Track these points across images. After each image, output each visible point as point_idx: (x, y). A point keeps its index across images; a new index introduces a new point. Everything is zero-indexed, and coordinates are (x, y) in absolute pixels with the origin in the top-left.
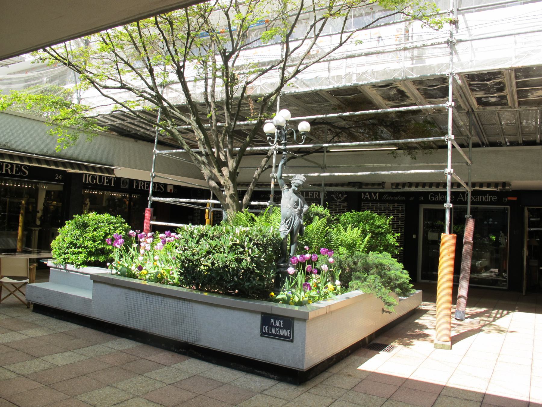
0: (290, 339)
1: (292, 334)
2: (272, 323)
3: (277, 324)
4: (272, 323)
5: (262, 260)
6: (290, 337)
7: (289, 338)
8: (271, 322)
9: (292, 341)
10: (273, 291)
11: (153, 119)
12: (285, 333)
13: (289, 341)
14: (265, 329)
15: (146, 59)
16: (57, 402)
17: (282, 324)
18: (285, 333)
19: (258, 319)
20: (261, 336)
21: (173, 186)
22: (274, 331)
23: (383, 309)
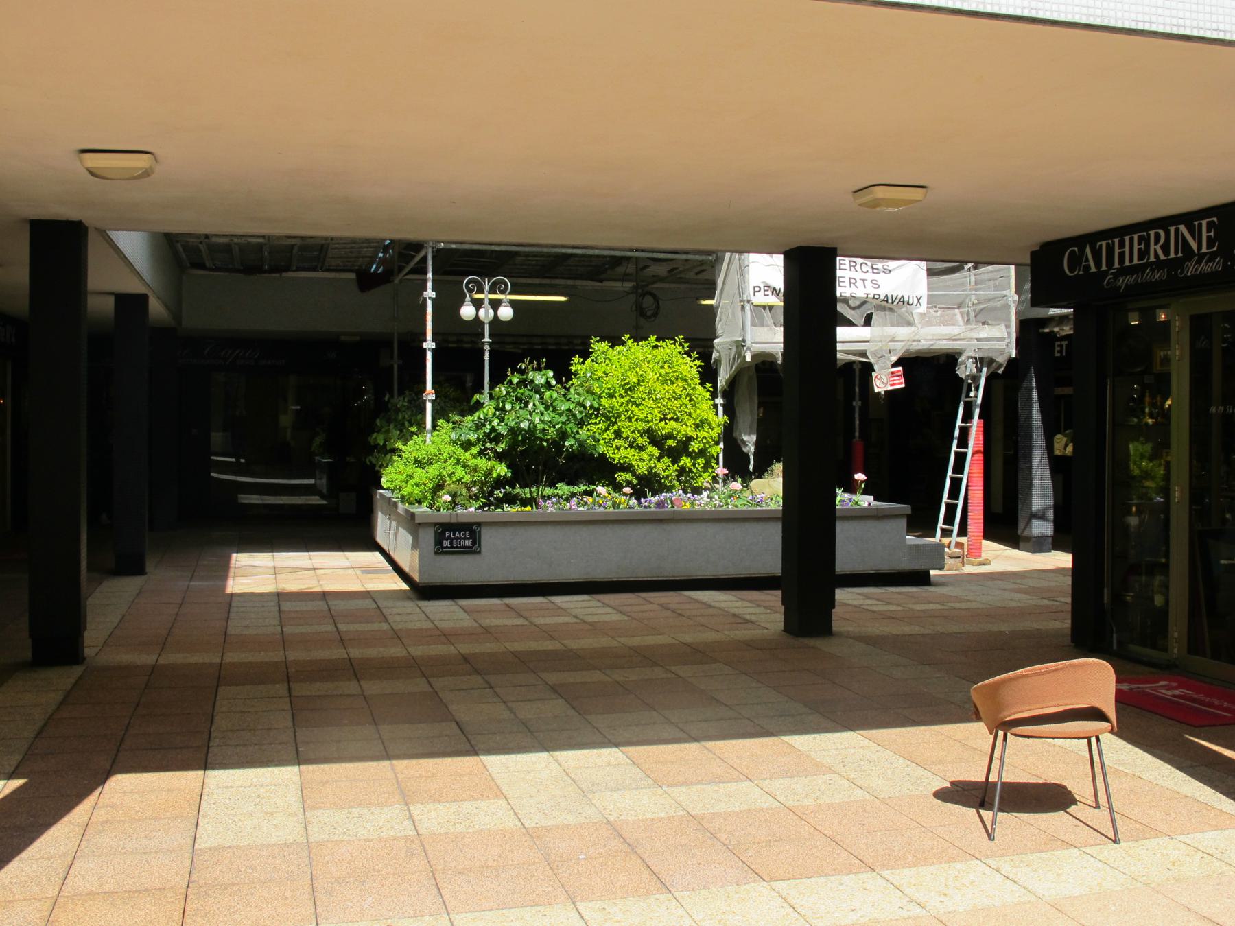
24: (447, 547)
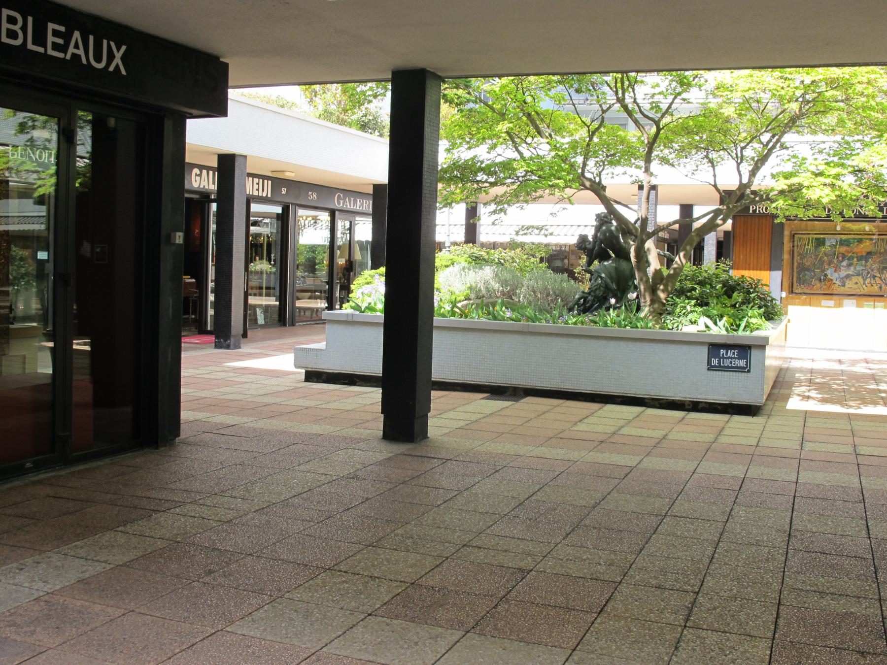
0: (746, 370)
1: (749, 364)
2: (723, 354)
3: (729, 355)
4: (723, 354)
5: (455, 172)
6: (747, 367)
7: (745, 368)
8: (721, 353)
9: (749, 371)
10: (615, 296)
11: (619, 80)
12: (742, 363)
13: (745, 372)
14: (715, 362)
15: (730, 152)
16: (382, 538)
17: (736, 354)
18: (742, 363)
19: (705, 350)
20: (708, 369)
21: (822, 305)
22: (727, 363)
23: (705, 323)
24: (715, 366)
